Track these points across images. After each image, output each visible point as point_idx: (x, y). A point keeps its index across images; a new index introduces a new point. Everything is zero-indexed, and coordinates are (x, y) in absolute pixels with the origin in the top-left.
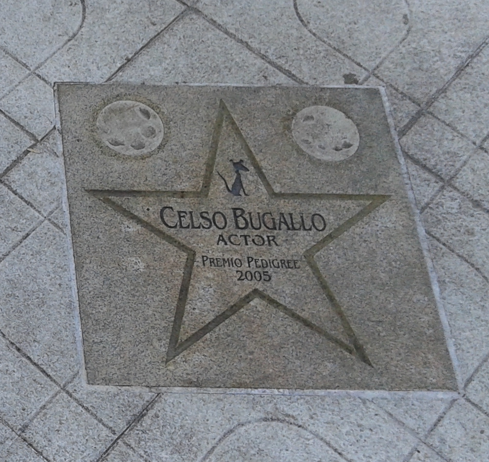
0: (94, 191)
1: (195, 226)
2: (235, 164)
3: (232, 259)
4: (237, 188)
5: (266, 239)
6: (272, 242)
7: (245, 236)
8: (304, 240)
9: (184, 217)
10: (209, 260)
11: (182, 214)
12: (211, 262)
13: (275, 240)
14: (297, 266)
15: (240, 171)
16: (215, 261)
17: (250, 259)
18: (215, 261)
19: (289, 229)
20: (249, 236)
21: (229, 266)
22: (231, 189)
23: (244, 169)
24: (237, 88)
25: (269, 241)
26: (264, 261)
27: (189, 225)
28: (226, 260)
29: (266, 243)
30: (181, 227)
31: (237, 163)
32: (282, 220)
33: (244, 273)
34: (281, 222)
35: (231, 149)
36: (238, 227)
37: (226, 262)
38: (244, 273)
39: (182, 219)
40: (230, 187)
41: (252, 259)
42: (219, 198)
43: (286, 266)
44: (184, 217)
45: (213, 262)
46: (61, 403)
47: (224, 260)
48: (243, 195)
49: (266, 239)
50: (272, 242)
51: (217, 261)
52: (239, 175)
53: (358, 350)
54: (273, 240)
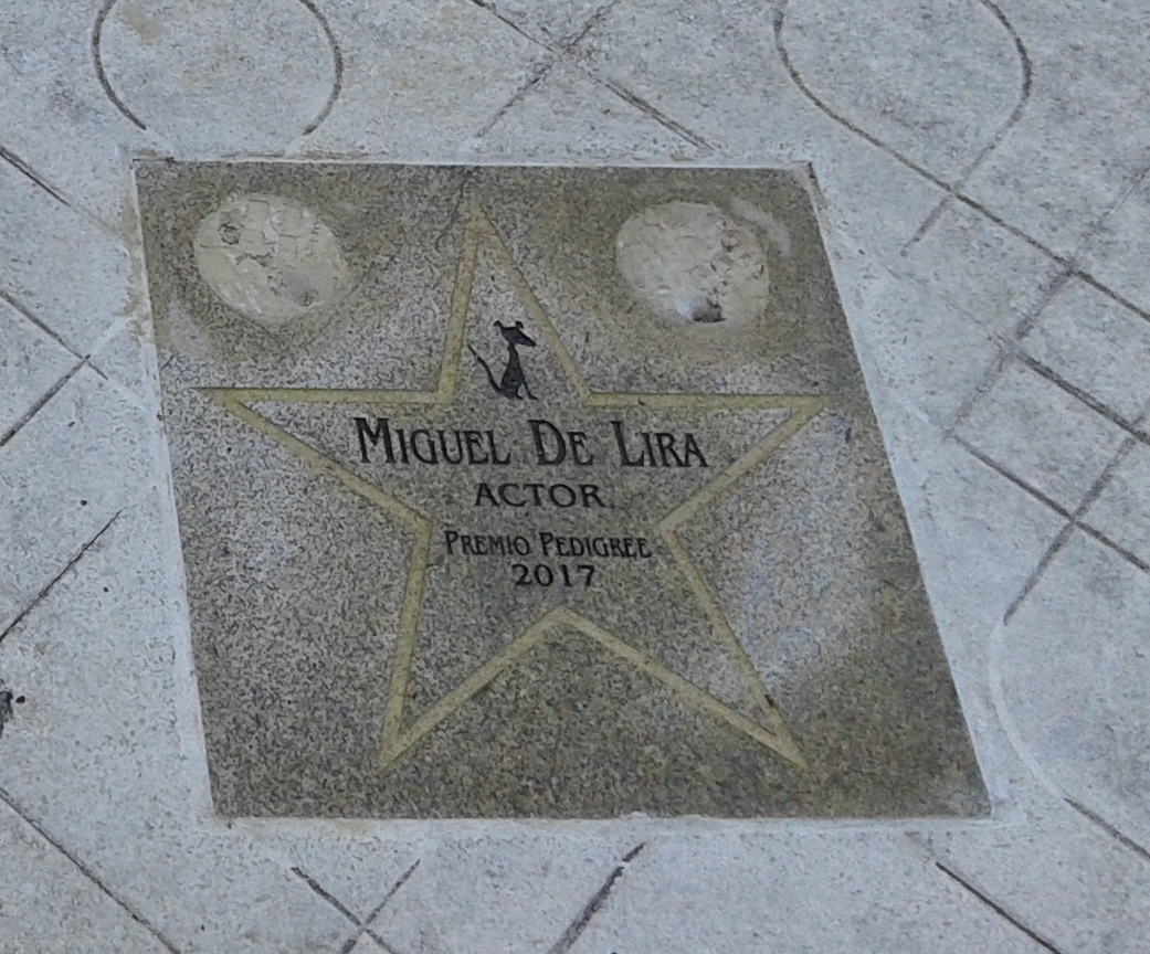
1: (631, 460)
2: (505, 330)
3: (587, 539)
5: (577, 491)
6: (590, 499)
9: (580, 443)
11: (474, 437)
14: (645, 552)
16: (473, 542)
17: (452, 537)
18: (473, 542)
20: (542, 486)
22: (498, 381)
23: (522, 340)
24: (562, 169)
25: (586, 496)
26: (575, 543)
29: (579, 498)
30: (496, 461)
32: (692, 448)
33: (531, 570)
34: (688, 451)
36: (543, 460)
38: (531, 570)
40: (498, 381)
44: (476, 441)
45: (469, 544)
49: (577, 491)
50: (590, 499)
51: (478, 543)
52: (514, 354)
54: (594, 495)
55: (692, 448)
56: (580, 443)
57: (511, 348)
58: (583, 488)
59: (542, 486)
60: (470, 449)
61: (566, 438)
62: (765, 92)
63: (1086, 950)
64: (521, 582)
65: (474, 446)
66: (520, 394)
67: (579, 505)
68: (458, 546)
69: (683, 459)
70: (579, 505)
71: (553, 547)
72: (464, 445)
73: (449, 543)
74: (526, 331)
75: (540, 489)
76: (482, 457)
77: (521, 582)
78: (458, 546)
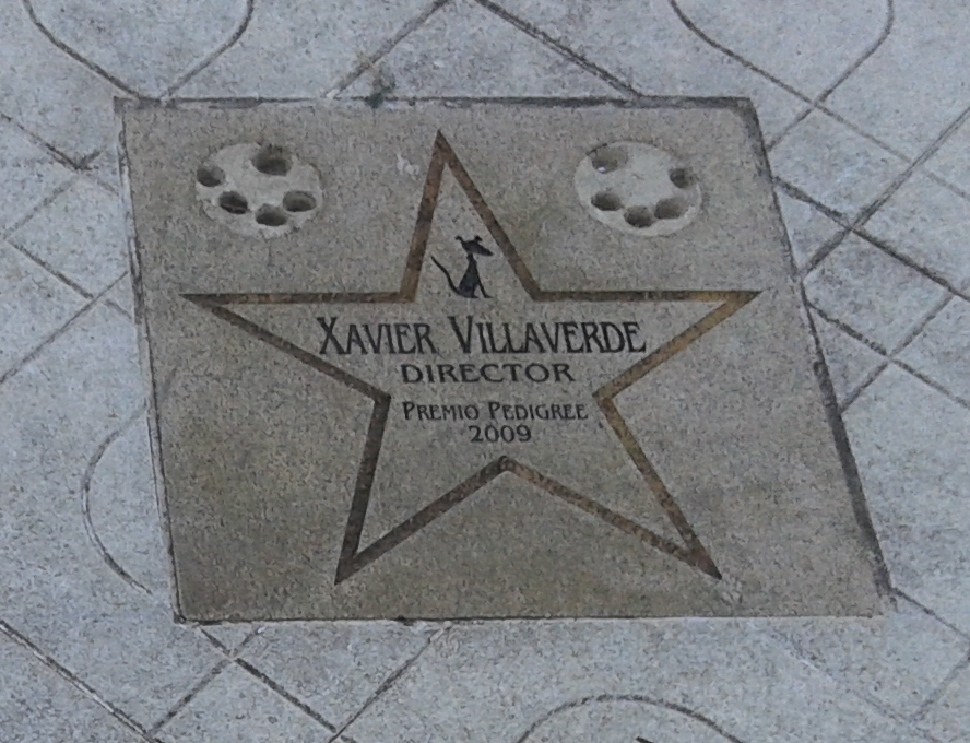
0: (200, 296)
2: (464, 244)
4: (470, 285)
5: (550, 369)
7: (513, 367)
8: (593, 368)
9: (573, 332)
10: (416, 408)
11: (631, 327)
12: (420, 413)
13: (569, 372)
15: (475, 256)
16: (562, 410)
19: (602, 350)
20: (520, 366)
21: (454, 418)
25: (441, 374)
27: (414, 348)
28: (448, 408)
29: (552, 375)
31: (471, 243)
35: (456, 218)
37: (449, 412)
39: (632, 336)
41: (498, 406)
42: (434, 302)
43: (562, 417)
46: (263, 722)
47: (444, 408)
48: (481, 296)
49: (550, 369)
51: (432, 412)
53: (696, 555)
54: (565, 372)
55: (531, 335)
56: (405, 333)
57: (470, 257)
58: (555, 366)
59: (520, 366)
60: (567, 340)
61: (622, 330)
62: (414, 79)
63: (4, 683)
64: (476, 439)
65: (632, 336)
66: (476, 294)
67: (551, 381)
68: (414, 414)
69: (345, 348)
70: (551, 381)
71: (499, 412)
72: (394, 337)
73: (406, 412)
74: (483, 244)
75: (517, 369)
76: (579, 346)
77: (476, 439)
78: (414, 414)
